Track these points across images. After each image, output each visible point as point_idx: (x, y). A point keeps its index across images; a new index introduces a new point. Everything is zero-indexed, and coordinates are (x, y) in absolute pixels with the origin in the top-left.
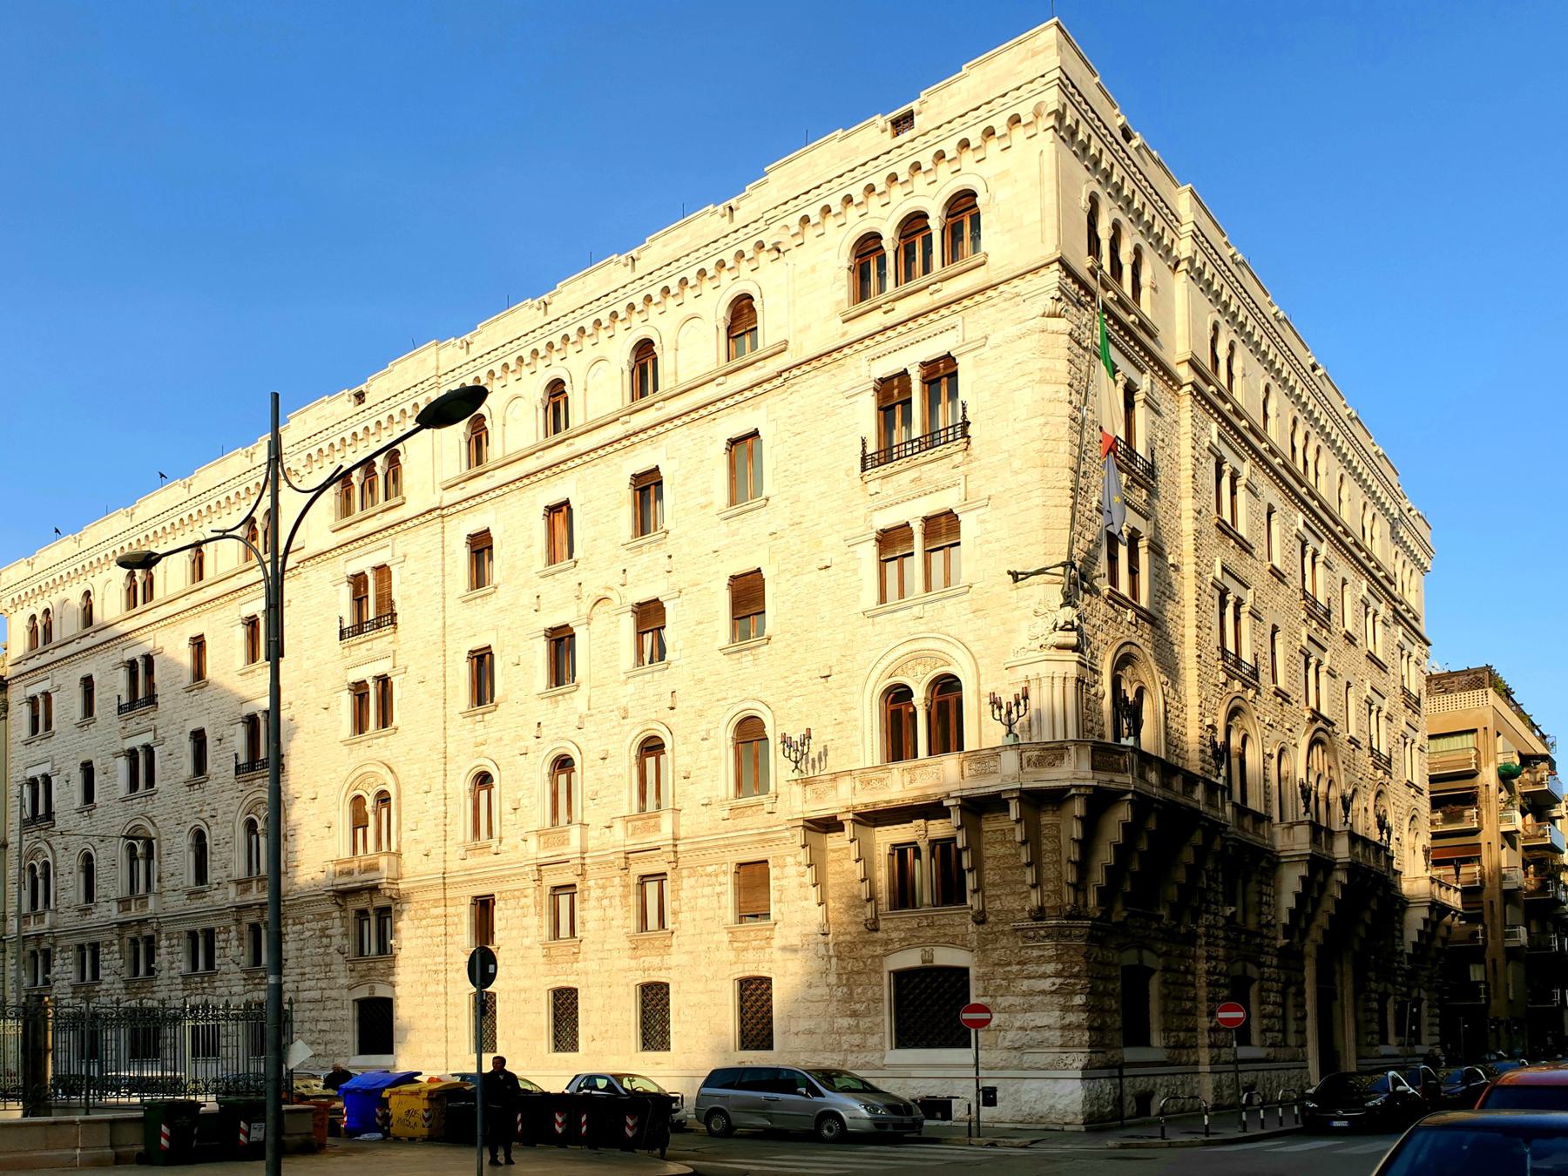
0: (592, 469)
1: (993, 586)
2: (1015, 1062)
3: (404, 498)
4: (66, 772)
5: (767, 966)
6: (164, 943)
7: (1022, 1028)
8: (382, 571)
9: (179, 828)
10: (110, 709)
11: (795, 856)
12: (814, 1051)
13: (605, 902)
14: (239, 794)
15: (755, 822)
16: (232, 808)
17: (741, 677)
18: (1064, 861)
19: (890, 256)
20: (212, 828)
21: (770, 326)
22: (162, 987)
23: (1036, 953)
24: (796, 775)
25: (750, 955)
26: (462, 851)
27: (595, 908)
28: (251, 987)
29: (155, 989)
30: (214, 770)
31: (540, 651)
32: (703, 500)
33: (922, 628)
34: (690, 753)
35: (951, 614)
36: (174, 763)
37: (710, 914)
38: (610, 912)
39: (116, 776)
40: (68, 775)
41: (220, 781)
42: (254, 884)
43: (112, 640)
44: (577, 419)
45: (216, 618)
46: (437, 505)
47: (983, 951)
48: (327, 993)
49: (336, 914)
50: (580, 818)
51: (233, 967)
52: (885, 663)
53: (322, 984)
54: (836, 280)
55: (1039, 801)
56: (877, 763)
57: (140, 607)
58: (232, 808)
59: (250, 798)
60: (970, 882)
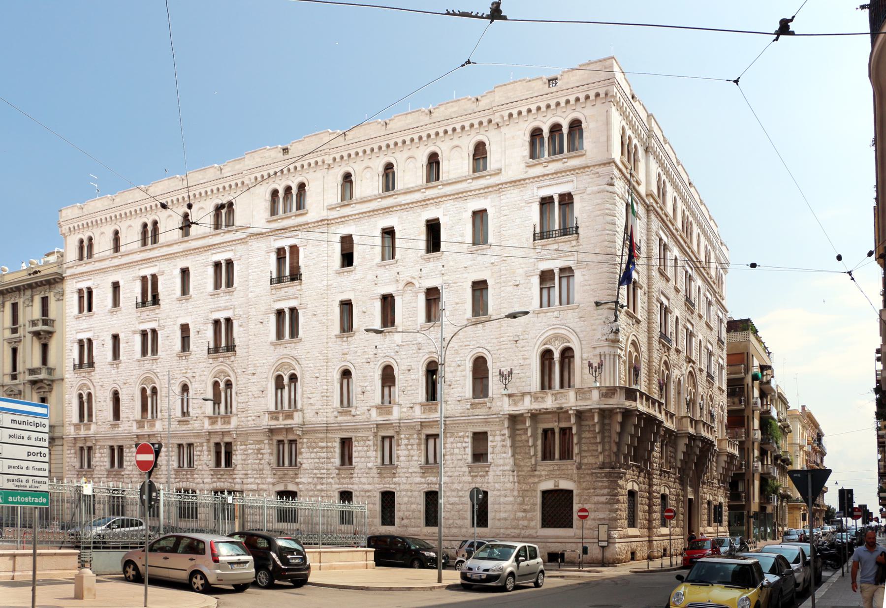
0: (406, 213)
4: (102, 338)
5: (486, 485)
7: (594, 520)
10: (130, 304)
11: (501, 431)
12: (507, 528)
13: (409, 447)
14: (209, 365)
16: (205, 373)
19: (546, 140)
21: (493, 160)
23: (600, 484)
24: (506, 392)
25: (479, 479)
27: (404, 450)
30: (196, 349)
31: (377, 307)
33: (559, 322)
34: (452, 372)
36: (170, 341)
37: (460, 457)
38: (412, 452)
39: (134, 345)
41: (198, 356)
43: (132, 263)
44: (399, 185)
47: (580, 482)
48: (261, 486)
49: (266, 442)
51: (205, 467)
52: (543, 338)
53: (258, 481)
55: (606, 414)
57: (149, 246)
58: (205, 373)
59: (217, 369)
60: (576, 450)
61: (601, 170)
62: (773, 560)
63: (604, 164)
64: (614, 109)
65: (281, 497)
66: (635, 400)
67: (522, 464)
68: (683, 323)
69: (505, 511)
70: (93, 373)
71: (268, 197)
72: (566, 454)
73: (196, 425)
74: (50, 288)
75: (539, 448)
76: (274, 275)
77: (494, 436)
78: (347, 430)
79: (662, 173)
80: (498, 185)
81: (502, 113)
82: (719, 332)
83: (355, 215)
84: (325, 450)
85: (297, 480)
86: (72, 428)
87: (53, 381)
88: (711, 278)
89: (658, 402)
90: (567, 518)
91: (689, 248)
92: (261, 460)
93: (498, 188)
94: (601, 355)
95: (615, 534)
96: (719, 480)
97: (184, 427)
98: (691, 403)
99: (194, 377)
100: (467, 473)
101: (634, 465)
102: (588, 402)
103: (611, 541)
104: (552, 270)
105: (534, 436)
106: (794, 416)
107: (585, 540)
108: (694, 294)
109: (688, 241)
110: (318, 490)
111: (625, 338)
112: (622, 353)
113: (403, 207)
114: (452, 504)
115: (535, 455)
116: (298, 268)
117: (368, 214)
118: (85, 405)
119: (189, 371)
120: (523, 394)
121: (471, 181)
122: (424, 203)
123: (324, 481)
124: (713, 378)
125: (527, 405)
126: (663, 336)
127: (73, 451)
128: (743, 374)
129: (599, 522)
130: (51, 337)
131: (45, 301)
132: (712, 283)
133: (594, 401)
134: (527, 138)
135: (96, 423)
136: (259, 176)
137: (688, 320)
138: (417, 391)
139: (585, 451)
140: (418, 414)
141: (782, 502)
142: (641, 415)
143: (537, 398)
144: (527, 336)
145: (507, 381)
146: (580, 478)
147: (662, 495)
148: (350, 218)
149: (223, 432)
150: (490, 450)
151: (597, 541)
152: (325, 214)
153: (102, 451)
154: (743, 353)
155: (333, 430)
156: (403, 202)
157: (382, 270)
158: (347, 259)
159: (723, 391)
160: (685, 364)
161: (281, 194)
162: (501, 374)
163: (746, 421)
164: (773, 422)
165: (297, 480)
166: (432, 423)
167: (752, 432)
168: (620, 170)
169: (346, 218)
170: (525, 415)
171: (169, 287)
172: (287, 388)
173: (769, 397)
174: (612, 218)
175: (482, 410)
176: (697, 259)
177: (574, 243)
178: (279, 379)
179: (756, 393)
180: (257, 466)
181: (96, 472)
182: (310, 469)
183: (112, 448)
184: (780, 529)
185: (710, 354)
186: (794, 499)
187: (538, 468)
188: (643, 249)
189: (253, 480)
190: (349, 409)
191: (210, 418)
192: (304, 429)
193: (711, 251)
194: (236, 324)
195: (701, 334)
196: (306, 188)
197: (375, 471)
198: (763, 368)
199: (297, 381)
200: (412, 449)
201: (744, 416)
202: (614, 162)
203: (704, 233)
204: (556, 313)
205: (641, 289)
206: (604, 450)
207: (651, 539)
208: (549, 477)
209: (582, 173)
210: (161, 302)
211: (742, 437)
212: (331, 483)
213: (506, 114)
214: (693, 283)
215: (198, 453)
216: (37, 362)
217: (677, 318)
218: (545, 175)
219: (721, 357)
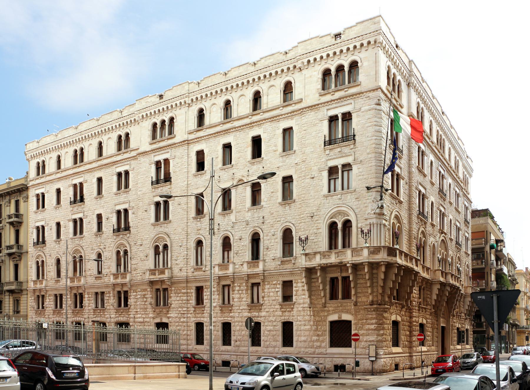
0: (239, 133)
1: (361, 191)
2: (364, 352)
3: (175, 135)
4: (50, 225)
6: (86, 296)
7: (366, 341)
8: (167, 161)
9: (92, 251)
10: (67, 202)
11: (301, 280)
12: (306, 348)
13: (240, 292)
15: (288, 267)
17: (285, 214)
18: (379, 286)
20: (104, 252)
22: (86, 313)
23: (370, 316)
24: (303, 252)
25: (287, 314)
26: (192, 270)
28: (118, 315)
29: (83, 314)
30: (105, 230)
32: (274, 148)
33: (341, 203)
35: (350, 199)
36: (90, 226)
37: (274, 298)
39: (69, 229)
40: (51, 226)
41: (107, 234)
42: (120, 275)
44: (235, 115)
45: (106, 171)
46: (186, 139)
48: (146, 320)
49: (149, 290)
50: (232, 260)
51: (111, 307)
53: (143, 316)
54: (317, 82)
55: (374, 266)
56: (327, 250)
60: (353, 292)
61: (371, 94)
62: (477, 381)
63: (374, 90)
64: (381, 53)
65: (158, 328)
66: (396, 256)
67: (316, 302)
68: (437, 206)
69: (305, 336)
70: (44, 248)
71: (150, 127)
72: (347, 295)
73: (106, 279)
74: (20, 194)
75: (328, 291)
76: (154, 179)
77: (297, 283)
78: (200, 281)
79: (420, 102)
80: (300, 109)
81: (303, 60)
82: (466, 215)
83: (205, 136)
84: (186, 295)
85: (168, 315)
86: (32, 283)
87: (21, 253)
88: (459, 178)
89: (415, 258)
90: (348, 341)
91: (442, 156)
92: (145, 302)
93: (300, 112)
94: (370, 225)
95: (381, 352)
96: (465, 314)
97: (99, 281)
98: (443, 261)
99: (105, 248)
100: (279, 310)
101: (396, 303)
102: (361, 258)
103: (379, 357)
104: (337, 166)
105: (324, 283)
106: (521, 274)
108: (446, 187)
109: (442, 152)
110: (182, 322)
111: (389, 213)
112: (387, 223)
113: (237, 129)
114: (269, 331)
115: (325, 296)
116: (169, 174)
117: (214, 135)
118: (40, 267)
119: (102, 244)
120: (315, 253)
121: (282, 108)
122: (251, 125)
123: (185, 316)
124: (460, 245)
125: (317, 261)
126: (421, 213)
127: (33, 298)
128: (483, 245)
129: (370, 343)
130: (20, 225)
131: (17, 203)
132: (460, 182)
133: (364, 257)
134: (320, 76)
135: (47, 280)
136: (144, 114)
137: (441, 205)
138: (245, 254)
139: (359, 293)
140: (246, 269)
141: (512, 328)
142: (400, 267)
143: (325, 256)
144: (319, 213)
145: (304, 245)
146: (356, 312)
147: (420, 324)
148: (202, 138)
149: (122, 284)
150: (294, 293)
151: (368, 357)
152: (186, 137)
153: (50, 298)
154: (484, 231)
155: (191, 281)
156: (237, 126)
157: (223, 172)
158: (201, 166)
159: (469, 255)
160: (439, 235)
161: (159, 126)
162: (300, 239)
164: (505, 276)
165: (168, 315)
166: (255, 275)
167: (490, 283)
168: (386, 95)
169: (200, 139)
170: (316, 268)
171: (90, 190)
172: (161, 254)
173: (502, 260)
174: (378, 128)
176: (448, 164)
177: (352, 146)
178: (157, 248)
179: (493, 258)
180: (143, 306)
181: (47, 312)
182: (176, 308)
183: (56, 296)
184: (511, 346)
185: (458, 229)
186: (521, 326)
187: (327, 305)
188: (405, 152)
189: (140, 315)
190: (201, 267)
191: (114, 275)
192: (172, 281)
193: (460, 160)
194: (130, 212)
195: (451, 215)
196: (175, 121)
197: (218, 308)
198: (498, 241)
199: (168, 249)
200: (242, 293)
201: (485, 272)
202: (380, 88)
203: (454, 148)
204: (339, 196)
205: (403, 180)
206: (372, 292)
207: (411, 355)
208: (334, 312)
209: (358, 97)
210: (85, 200)
211: (483, 286)
212: (190, 317)
213: (305, 61)
214: (445, 180)
215: (107, 298)
216: (13, 242)
217: (432, 203)
218: (332, 101)
219: (467, 233)
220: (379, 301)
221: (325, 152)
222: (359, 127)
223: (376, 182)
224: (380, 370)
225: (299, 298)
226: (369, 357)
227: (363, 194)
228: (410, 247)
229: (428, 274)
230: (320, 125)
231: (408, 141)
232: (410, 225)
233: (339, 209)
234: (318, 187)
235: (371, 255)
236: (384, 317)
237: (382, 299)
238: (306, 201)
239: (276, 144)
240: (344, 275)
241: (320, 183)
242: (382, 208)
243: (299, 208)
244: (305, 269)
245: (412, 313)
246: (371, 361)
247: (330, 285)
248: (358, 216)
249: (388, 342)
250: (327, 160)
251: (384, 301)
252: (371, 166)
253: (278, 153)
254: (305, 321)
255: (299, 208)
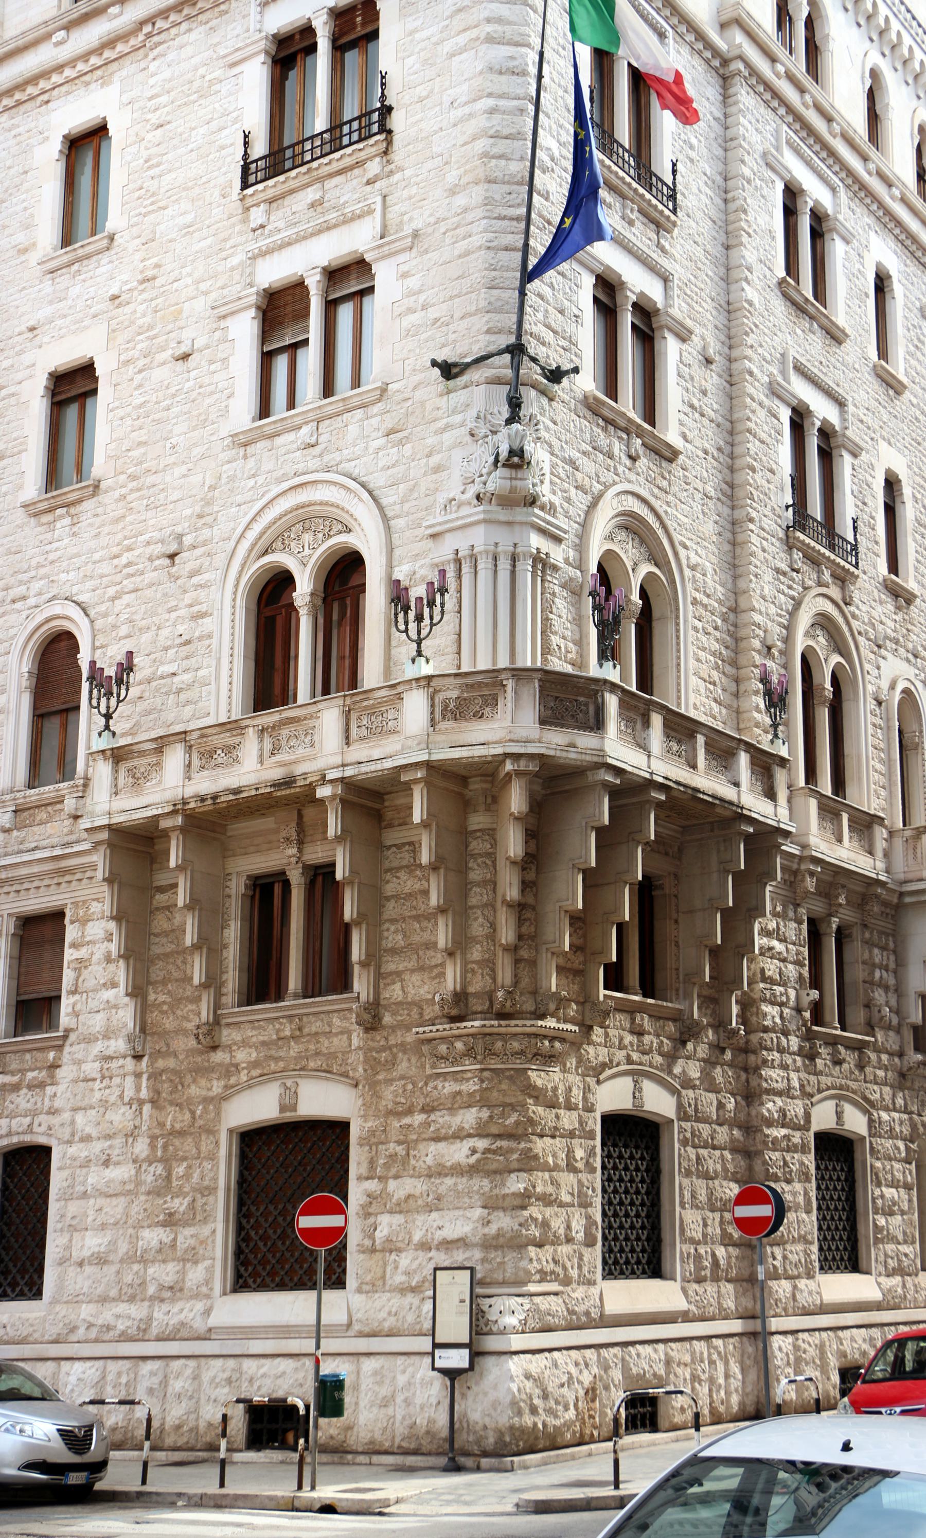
7: (425, 1246)
12: (104, 1300)
17: (52, 557)
23: (449, 1087)
32: (21, 238)
33: (313, 464)
66: (597, 724)
67: (169, 1023)
69: (103, 1227)
77: (83, 922)
80: (142, 23)
103: (492, 1343)
107: (328, 1345)
111: (581, 501)
112: (557, 554)
115: (213, 982)
120: (161, 744)
121: (63, 33)
129: (442, 1259)
139: (394, 951)
143: (211, 754)
144: (206, 533)
145: (113, 701)
146: (373, 1065)
147: (819, 1136)
150: (68, 976)
151: (425, 1344)
163: (660, 533)
170: (165, 824)
175: (49, 828)
204: (305, 430)
217: (892, 485)
220: (500, 994)
221: (245, 221)
222: (409, 61)
223: (488, 332)
224: (500, 1433)
225: (93, 1004)
226: (436, 1346)
227: (423, 403)
228: (737, 695)
229: (871, 853)
230: (225, 88)
231: (719, 152)
232: (735, 578)
233: (303, 497)
234: (208, 401)
235: (444, 725)
236: (537, 1094)
237: (516, 983)
238: (150, 479)
239: (32, 216)
240: (316, 854)
241: (217, 378)
242: (517, 467)
243: (117, 520)
244: (105, 835)
245: (757, 1069)
246: (445, 1372)
247: (248, 919)
248: (396, 524)
249: (564, 1250)
250: (254, 258)
251: (534, 993)
252: (467, 254)
253: (34, 257)
254: (108, 1137)
255: (117, 520)
